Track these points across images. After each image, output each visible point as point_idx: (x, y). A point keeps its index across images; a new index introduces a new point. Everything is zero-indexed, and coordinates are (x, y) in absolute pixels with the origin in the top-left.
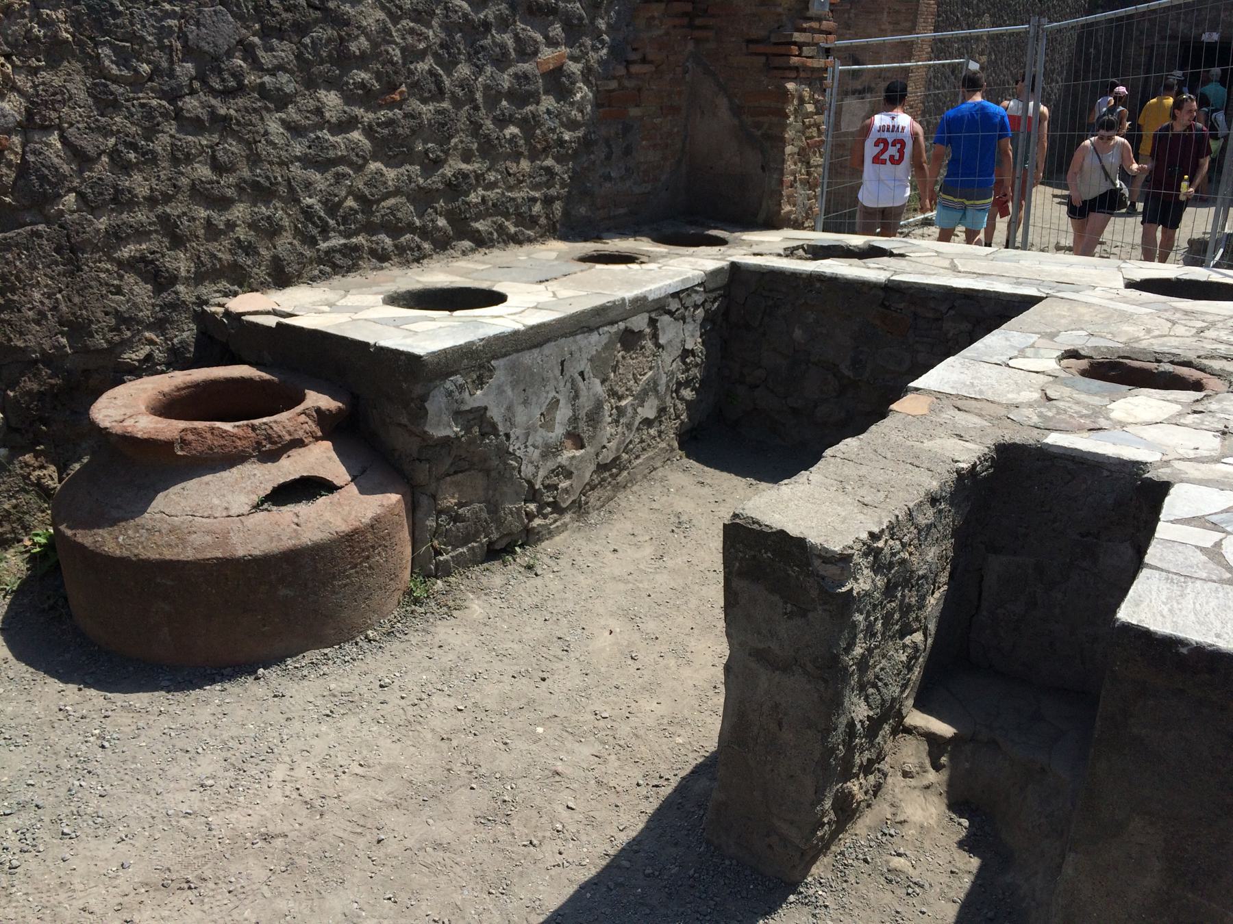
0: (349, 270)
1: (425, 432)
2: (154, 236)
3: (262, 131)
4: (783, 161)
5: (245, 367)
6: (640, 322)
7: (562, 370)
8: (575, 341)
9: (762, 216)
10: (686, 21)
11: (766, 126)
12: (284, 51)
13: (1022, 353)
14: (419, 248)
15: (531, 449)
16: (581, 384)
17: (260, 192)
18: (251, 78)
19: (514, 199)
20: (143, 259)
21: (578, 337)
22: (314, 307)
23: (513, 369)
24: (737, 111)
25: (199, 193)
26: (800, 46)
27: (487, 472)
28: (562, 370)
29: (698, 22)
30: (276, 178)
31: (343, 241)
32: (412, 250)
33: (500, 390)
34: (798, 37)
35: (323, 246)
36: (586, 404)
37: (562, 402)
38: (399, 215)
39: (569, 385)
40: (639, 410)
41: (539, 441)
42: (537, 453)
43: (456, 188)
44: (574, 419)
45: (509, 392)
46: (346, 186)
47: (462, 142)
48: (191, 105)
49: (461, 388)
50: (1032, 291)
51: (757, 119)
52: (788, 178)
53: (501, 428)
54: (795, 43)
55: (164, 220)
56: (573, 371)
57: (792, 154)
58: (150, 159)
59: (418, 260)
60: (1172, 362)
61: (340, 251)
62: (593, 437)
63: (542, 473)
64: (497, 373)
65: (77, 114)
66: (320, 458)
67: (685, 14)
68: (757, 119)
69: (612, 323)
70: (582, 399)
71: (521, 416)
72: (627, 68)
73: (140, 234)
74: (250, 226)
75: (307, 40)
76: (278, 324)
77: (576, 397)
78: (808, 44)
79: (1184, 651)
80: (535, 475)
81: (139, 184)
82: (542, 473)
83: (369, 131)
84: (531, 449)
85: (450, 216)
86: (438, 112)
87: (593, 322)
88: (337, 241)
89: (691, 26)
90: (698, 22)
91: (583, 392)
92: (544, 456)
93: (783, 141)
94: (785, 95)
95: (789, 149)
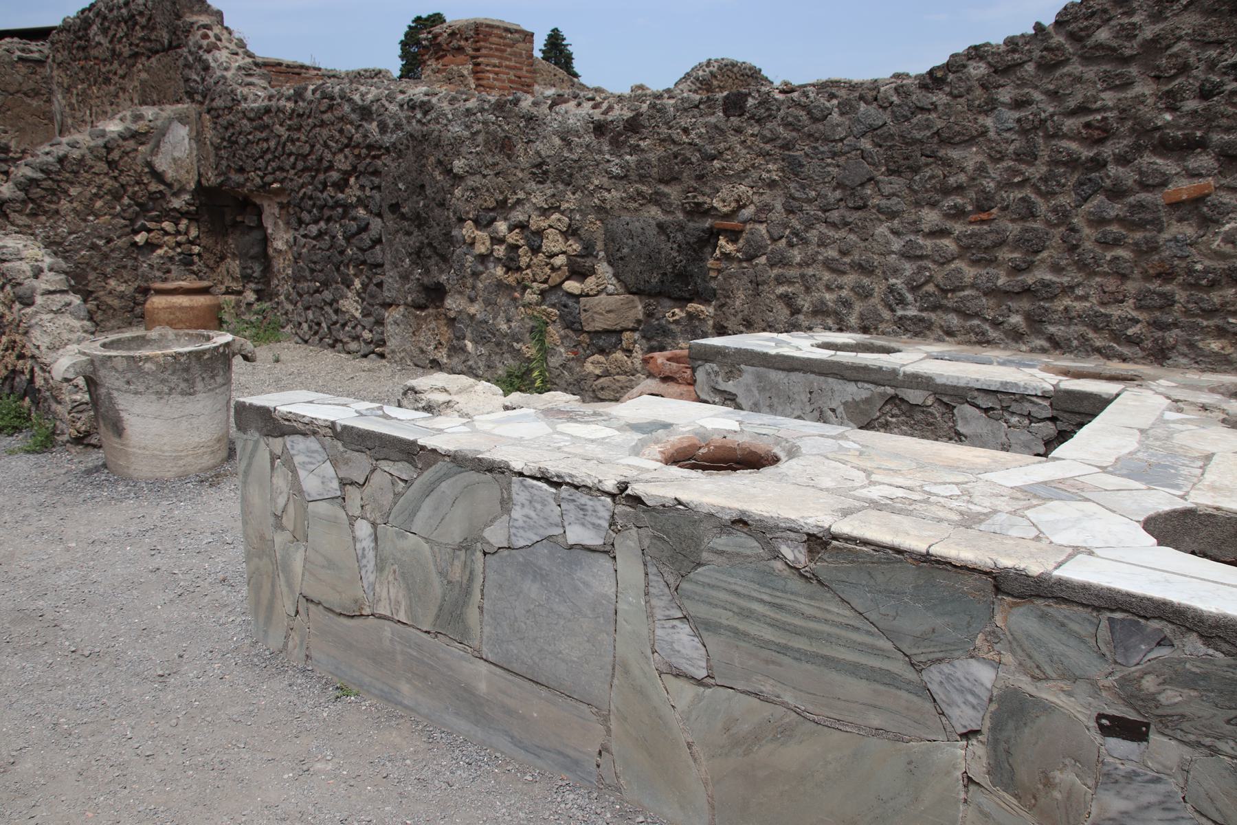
0: (916, 334)
12: (898, 183)
13: (317, 291)
17: (865, 269)
20: (787, 296)
23: (759, 378)
25: (829, 265)
31: (916, 313)
32: (977, 334)
33: (748, 390)
35: (900, 313)
38: (968, 304)
43: (1045, 292)
45: (756, 392)
47: (1052, 257)
55: (803, 276)
58: (805, 242)
61: (910, 319)
64: (745, 376)
65: (778, 213)
73: (790, 282)
74: (852, 289)
75: (917, 178)
81: (797, 255)
83: (958, 239)
85: (1028, 317)
87: (847, 374)
88: (912, 312)
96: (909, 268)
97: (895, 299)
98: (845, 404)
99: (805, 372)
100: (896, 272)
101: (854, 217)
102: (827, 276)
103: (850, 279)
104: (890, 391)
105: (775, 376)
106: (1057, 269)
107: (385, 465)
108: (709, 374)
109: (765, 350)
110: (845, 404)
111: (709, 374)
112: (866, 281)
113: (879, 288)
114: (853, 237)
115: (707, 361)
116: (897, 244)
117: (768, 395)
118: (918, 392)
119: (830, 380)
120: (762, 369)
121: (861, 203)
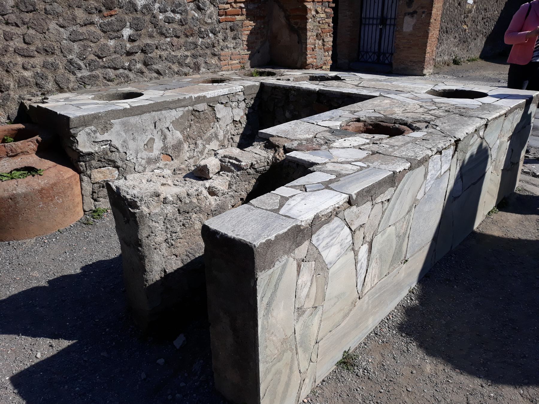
3: (46, 28)
5: (20, 124)
6: (201, 107)
7: (155, 126)
8: (161, 114)
9: (299, 65)
11: (299, 24)
14: (127, 77)
19: (176, 56)
23: (124, 124)
24: (287, 18)
28: (155, 126)
30: (54, 47)
31: (89, 73)
33: (118, 134)
35: (79, 75)
37: (156, 140)
39: (160, 133)
40: (207, 146)
41: (145, 157)
45: (123, 134)
46: (89, 51)
48: (12, 18)
49: (95, 132)
50: (364, 92)
51: (295, 21)
53: (120, 149)
59: (127, 82)
60: (400, 124)
62: (179, 156)
66: (33, 160)
68: (295, 21)
71: (132, 145)
76: (38, 106)
79: (218, 236)
84: (140, 160)
86: (134, 19)
94: (305, 8)
96: (76, 47)
97: (72, 67)
98: (173, 122)
99: (150, 112)
100: (70, 51)
101: (27, 17)
102: (20, 60)
103: (38, 60)
104: (191, 108)
105: (133, 120)
106: (151, 36)
107: (379, 200)
108: (89, 134)
109: (387, 77)
110: (173, 122)
111: (89, 134)
112: (50, 59)
113: (61, 63)
114: (31, 32)
115: (86, 126)
116: (65, 33)
117: (131, 133)
118: (201, 105)
119: (163, 112)
120: (125, 119)
121: (31, 8)
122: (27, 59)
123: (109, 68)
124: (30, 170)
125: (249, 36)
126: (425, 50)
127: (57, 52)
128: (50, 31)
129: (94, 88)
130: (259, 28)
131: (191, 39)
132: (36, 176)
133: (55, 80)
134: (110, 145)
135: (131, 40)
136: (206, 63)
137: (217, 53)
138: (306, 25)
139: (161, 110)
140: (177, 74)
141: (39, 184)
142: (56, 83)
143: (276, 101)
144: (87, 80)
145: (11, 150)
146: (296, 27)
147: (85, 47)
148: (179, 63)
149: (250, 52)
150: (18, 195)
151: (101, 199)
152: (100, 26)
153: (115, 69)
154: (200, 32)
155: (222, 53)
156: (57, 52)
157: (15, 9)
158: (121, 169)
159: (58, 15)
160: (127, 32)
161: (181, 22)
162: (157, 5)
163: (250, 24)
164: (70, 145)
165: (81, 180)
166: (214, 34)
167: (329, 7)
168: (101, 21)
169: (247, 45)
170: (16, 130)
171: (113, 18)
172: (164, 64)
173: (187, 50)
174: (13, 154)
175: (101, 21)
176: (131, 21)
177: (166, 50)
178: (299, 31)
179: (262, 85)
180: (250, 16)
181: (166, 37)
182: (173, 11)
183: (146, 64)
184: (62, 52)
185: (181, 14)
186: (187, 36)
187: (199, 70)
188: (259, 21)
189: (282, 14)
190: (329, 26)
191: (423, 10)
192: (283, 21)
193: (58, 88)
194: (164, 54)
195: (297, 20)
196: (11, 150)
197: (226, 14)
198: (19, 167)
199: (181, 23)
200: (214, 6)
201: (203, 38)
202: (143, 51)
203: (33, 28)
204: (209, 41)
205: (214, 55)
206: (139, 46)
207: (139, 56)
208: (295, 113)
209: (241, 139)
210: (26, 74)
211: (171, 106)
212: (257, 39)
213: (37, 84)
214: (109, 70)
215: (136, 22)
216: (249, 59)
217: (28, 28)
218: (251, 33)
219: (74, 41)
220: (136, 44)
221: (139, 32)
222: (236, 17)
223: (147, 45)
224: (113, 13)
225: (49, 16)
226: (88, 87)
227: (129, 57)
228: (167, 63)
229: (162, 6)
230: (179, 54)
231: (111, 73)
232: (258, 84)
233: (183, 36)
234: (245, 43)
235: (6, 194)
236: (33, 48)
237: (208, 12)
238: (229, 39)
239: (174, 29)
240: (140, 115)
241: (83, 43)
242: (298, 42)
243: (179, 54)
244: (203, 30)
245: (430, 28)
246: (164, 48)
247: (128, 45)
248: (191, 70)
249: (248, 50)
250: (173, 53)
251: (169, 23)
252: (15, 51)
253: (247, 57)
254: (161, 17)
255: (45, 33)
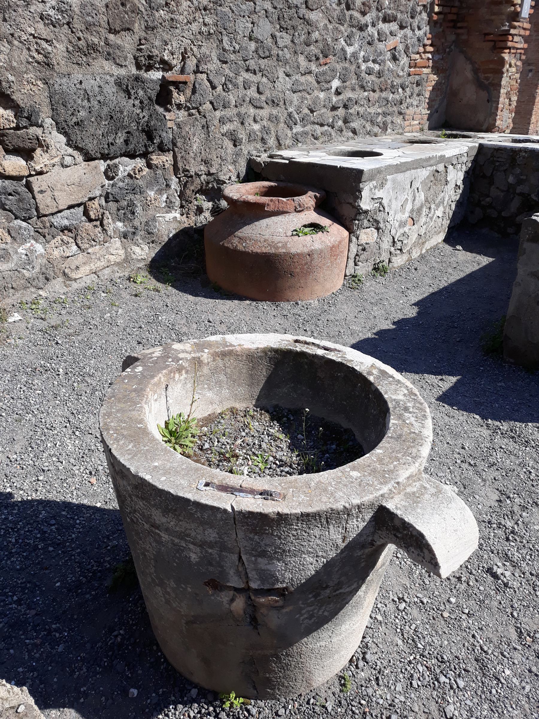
1: (359, 206)
2: (235, 123)
4: (499, 97)
9: (484, 128)
10: (451, 24)
11: (491, 79)
15: (395, 221)
16: (417, 194)
17: (274, 103)
18: (274, 52)
19: (370, 113)
21: (419, 170)
22: (300, 155)
23: (394, 181)
24: (476, 71)
26: (513, 35)
27: (378, 229)
29: (459, 25)
31: (302, 129)
34: (512, 31)
35: (294, 131)
36: (418, 204)
42: (397, 224)
44: (412, 211)
48: (252, 64)
51: (486, 75)
52: (501, 106)
54: (511, 35)
55: (239, 115)
56: (415, 186)
57: (503, 93)
63: (398, 234)
67: (452, 21)
68: (486, 75)
69: (431, 166)
70: (416, 201)
72: (424, 49)
77: (414, 200)
78: (516, 35)
80: (396, 235)
82: (398, 234)
84: (395, 221)
89: (455, 27)
90: (459, 25)
91: (417, 198)
92: (400, 226)
93: (500, 86)
94: (502, 62)
95: (502, 91)
96: (295, 98)
106: (353, 89)
121: (267, 54)
122: (257, 111)
123: (318, 124)
124: (315, 227)
125: (432, 92)
126: (529, 119)
127: (281, 103)
128: (279, 79)
129: (304, 147)
130: (441, 83)
131: (384, 95)
132: (325, 233)
133: (277, 135)
134: (381, 203)
135: (338, 93)
136: (392, 122)
137: (403, 111)
138: (501, 81)
139: (417, 168)
140: (368, 134)
141: (330, 241)
142: (277, 139)
143: (497, 164)
144: (299, 136)
145: (300, 205)
146: (486, 82)
147: (303, 98)
148: (371, 121)
149: (429, 112)
150: (316, 250)
151: (360, 263)
152: (316, 74)
153: (322, 125)
154: (393, 86)
155: (408, 112)
156: (281, 103)
157: (254, 54)
158: (381, 230)
159: (286, 62)
160: (336, 83)
161: (379, 73)
162: (362, 53)
163: (434, 78)
164: (351, 201)
165: (350, 241)
166: (403, 89)
167: (520, 59)
168: (317, 70)
169: (428, 103)
170: (267, 187)
171: (327, 67)
172: (359, 122)
173: (380, 107)
174: (301, 209)
175: (317, 70)
176: (340, 71)
177: (363, 105)
178: (490, 88)
179: (481, 145)
180: (436, 69)
181: (365, 91)
182: (374, 61)
183: (346, 121)
184: (285, 104)
185: (380, 65)
186: (381, 91)
187: (387, 130)
188: (441, 75)
189: (469, 67)
190: (517, 82)
191: (531, 68)
192: (469, 74)
193: (277, 145)
194: (361, 110)
195: (489, 75)
196: (300, 205)
197: (415, 67)
198: (307, 223)
199: (380, 74)
200: (407, 56)
201: (393, 93)
202: (346, 107)
203: (266, 76)
204: (397, 96)
205: (400, 113)
206: (343, 100)
207: (341, 112)
208: (522, 177)
209: (457, 206)
210: (255, 127)
211: (425, 164)
212: (437, 96)
213: (262, 139)
214: (317, 126)
215: (344, 72)
216: (428, 120)
217: (262, 76)
218: (433, 89)
219: (294, 92)
220: (341, 97)
221: (345, 84)
222: (424, 69)
223: (350, 99)
224: (328, 61)
225: (280, 63)
226: (300, 145)
227: (333, 113)
228: (362, 121)
229: (367, 55)
230: (372, 110)
231: (319, 130)
232: (477, 145)
233: (378, 90)
234: (427, 101)
235: (306, 250)
236: (263, 98)
237: (402, 63)
238: (415, 95)
239: (372, 81)
240: (404, 172)
241: (300, 95)
242: (488, 101)
243: (372, 110)
244: (395, 84)
245: (537, 91)
246: (362, 103)
247: (334, 99)
248: (380, 130)
249: (428, 109)
250: (368, 110)
251: (369, 74)
252: (250, 101)
253: (426, 117)
254: (363, 67)
255: (275, 82)
